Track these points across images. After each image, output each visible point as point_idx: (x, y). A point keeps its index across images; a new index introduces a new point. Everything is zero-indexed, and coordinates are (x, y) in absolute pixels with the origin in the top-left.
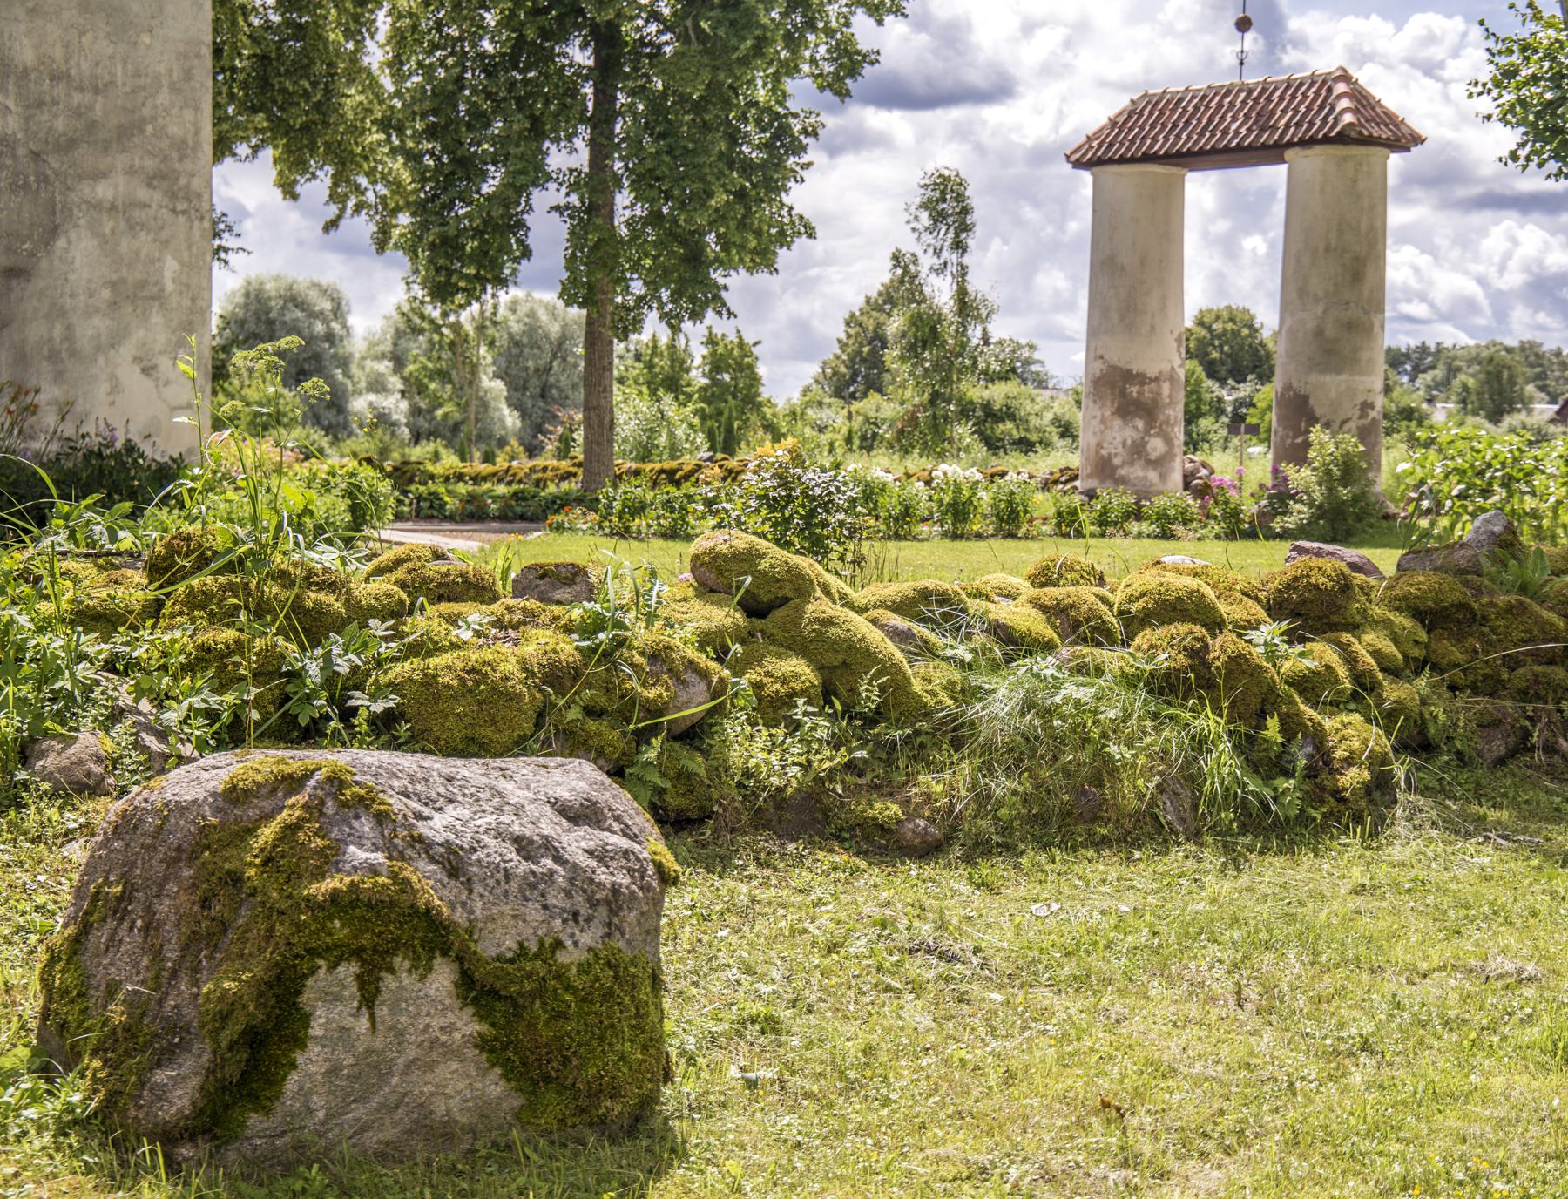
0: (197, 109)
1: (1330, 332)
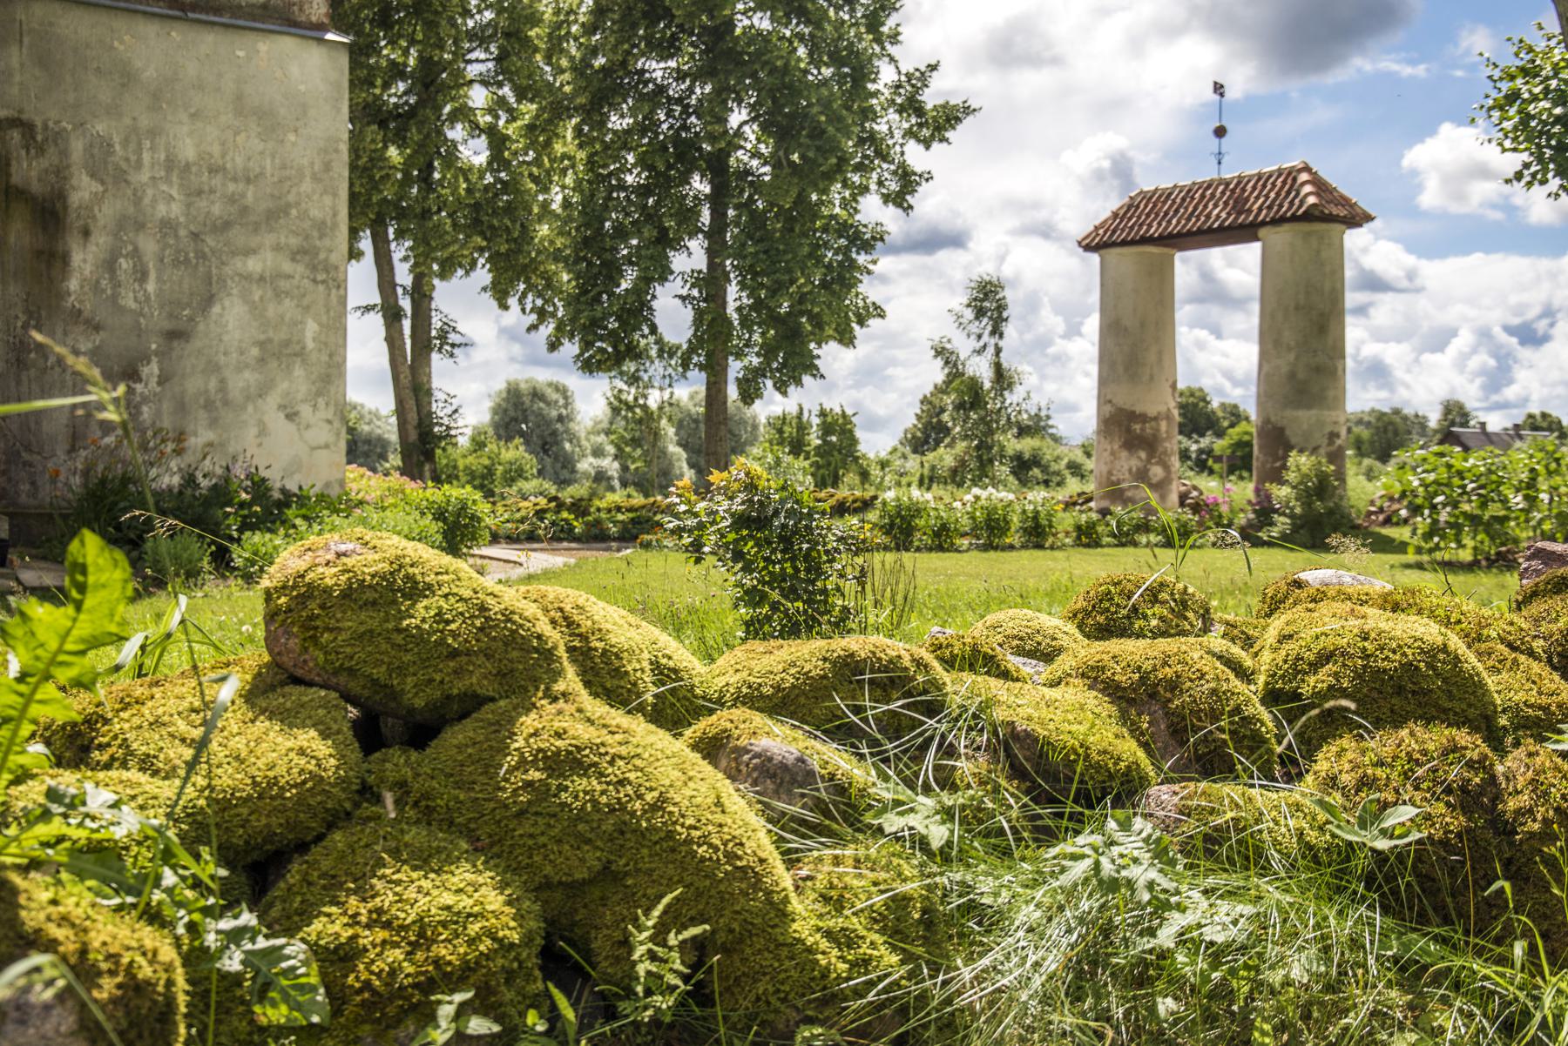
0: (335, 195)
1: (1301, 375)
